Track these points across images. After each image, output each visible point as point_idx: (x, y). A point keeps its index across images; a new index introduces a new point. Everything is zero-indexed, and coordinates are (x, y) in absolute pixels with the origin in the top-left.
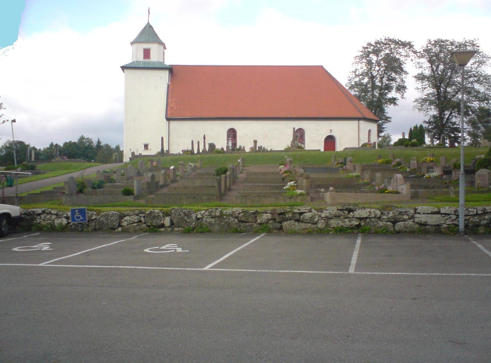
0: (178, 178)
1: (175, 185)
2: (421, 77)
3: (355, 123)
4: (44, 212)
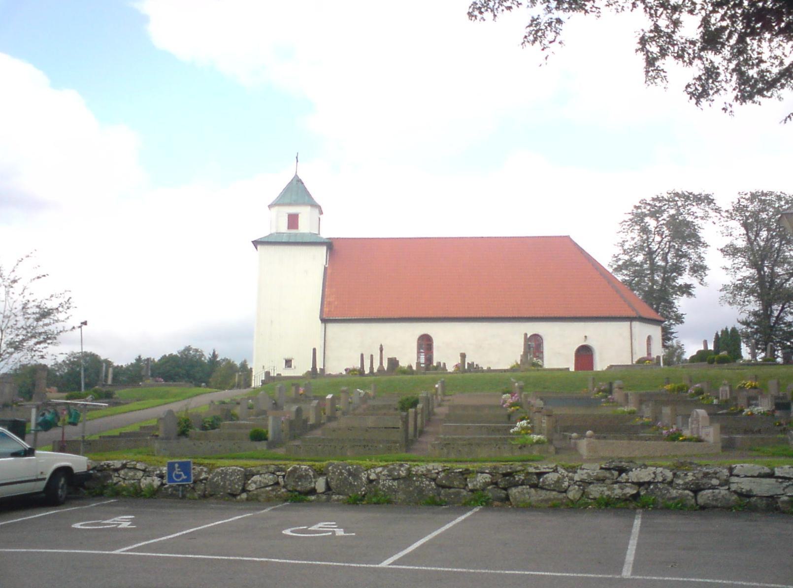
0: (339, 413)
1: (333, 424)
2: (731, 251)
3: (626, 324)
4: (124, 466)
